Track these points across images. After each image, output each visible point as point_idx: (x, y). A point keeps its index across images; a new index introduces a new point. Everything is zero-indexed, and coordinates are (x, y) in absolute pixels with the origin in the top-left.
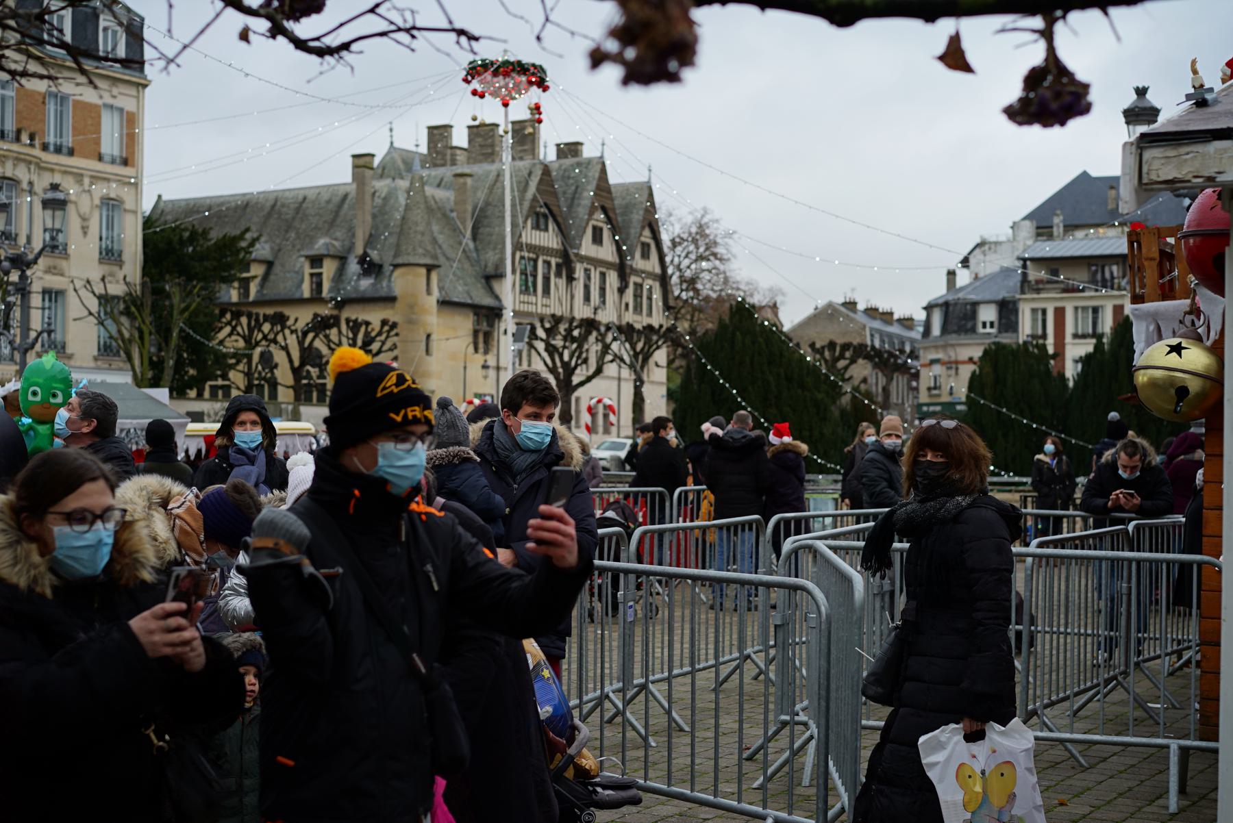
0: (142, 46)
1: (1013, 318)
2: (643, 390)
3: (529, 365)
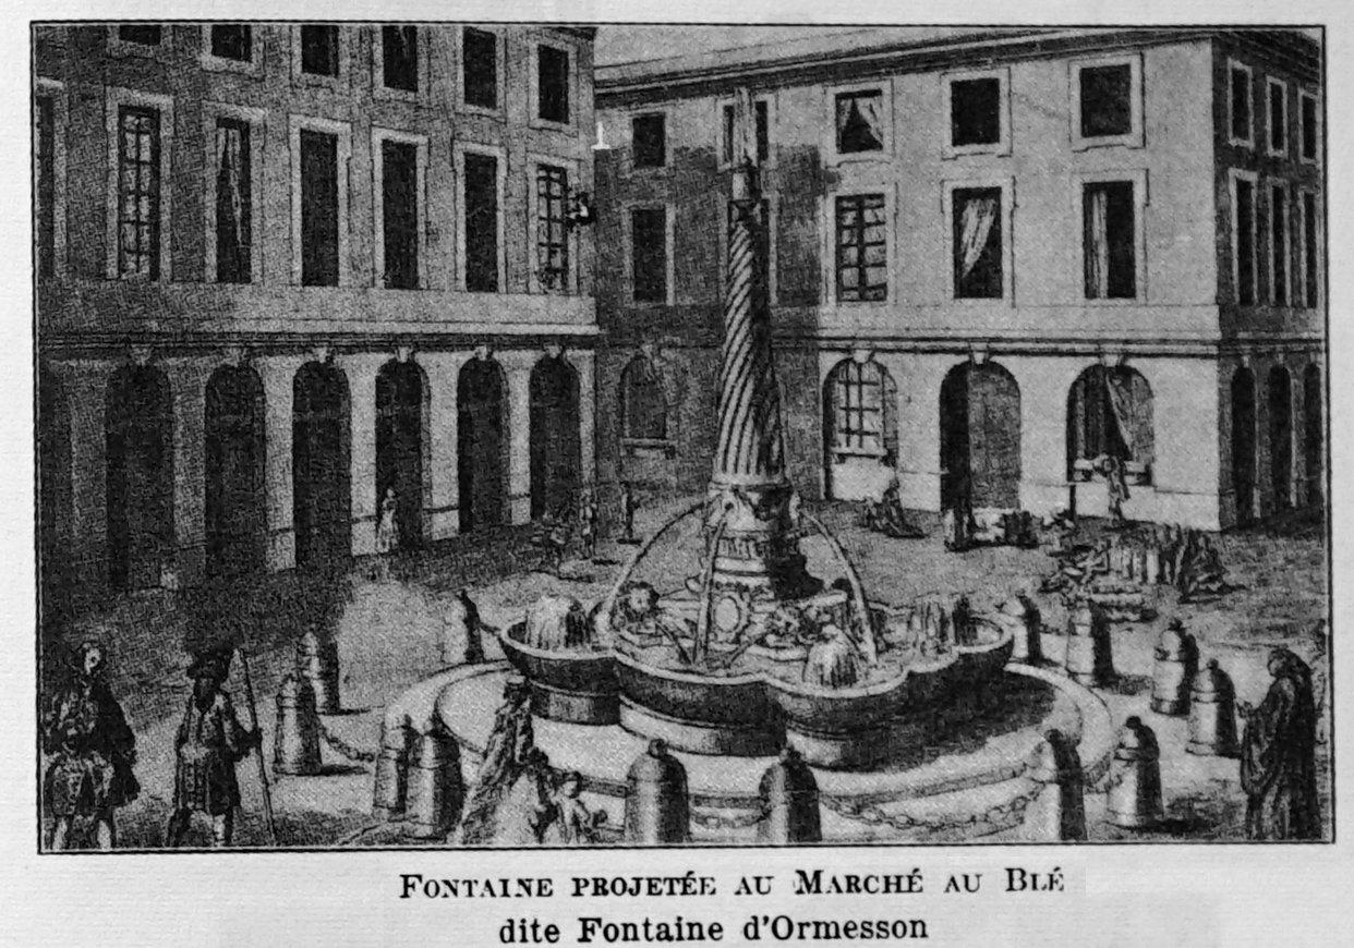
3: (861, 446)
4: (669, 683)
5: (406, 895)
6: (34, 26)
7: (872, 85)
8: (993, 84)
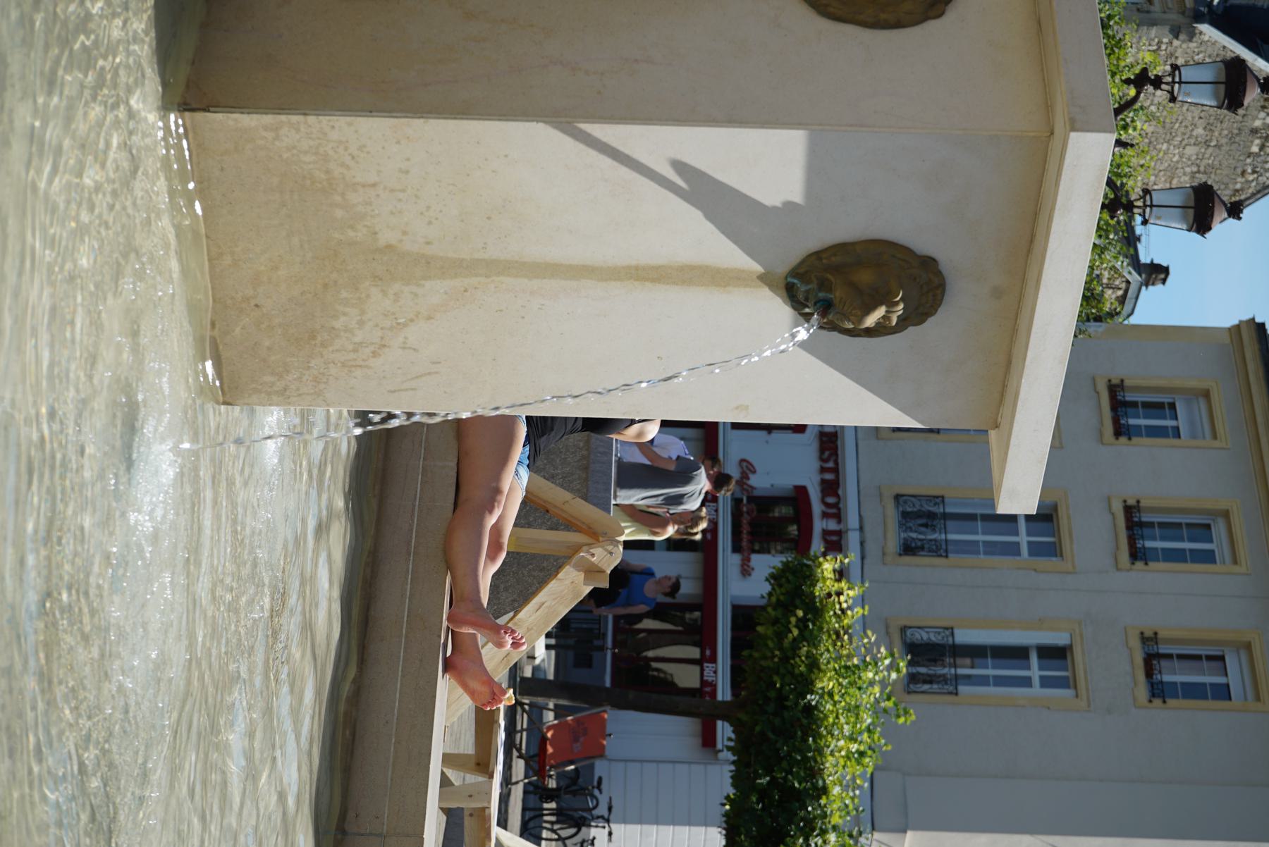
1: (1209, 219)
6: (951, 688)
7: (1242, 552)
8: (736, 608)
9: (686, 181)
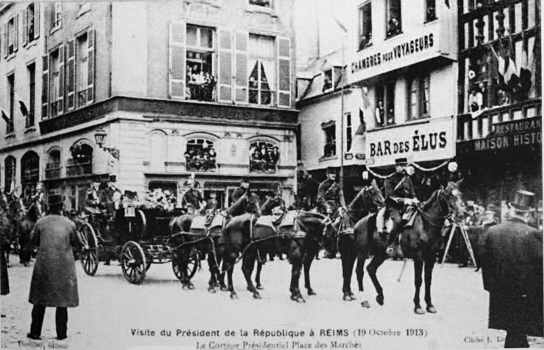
0: (313, 259)
2: (291, 266)
4: (198, 31)
5: (293, 347)
9: (147, 221)
